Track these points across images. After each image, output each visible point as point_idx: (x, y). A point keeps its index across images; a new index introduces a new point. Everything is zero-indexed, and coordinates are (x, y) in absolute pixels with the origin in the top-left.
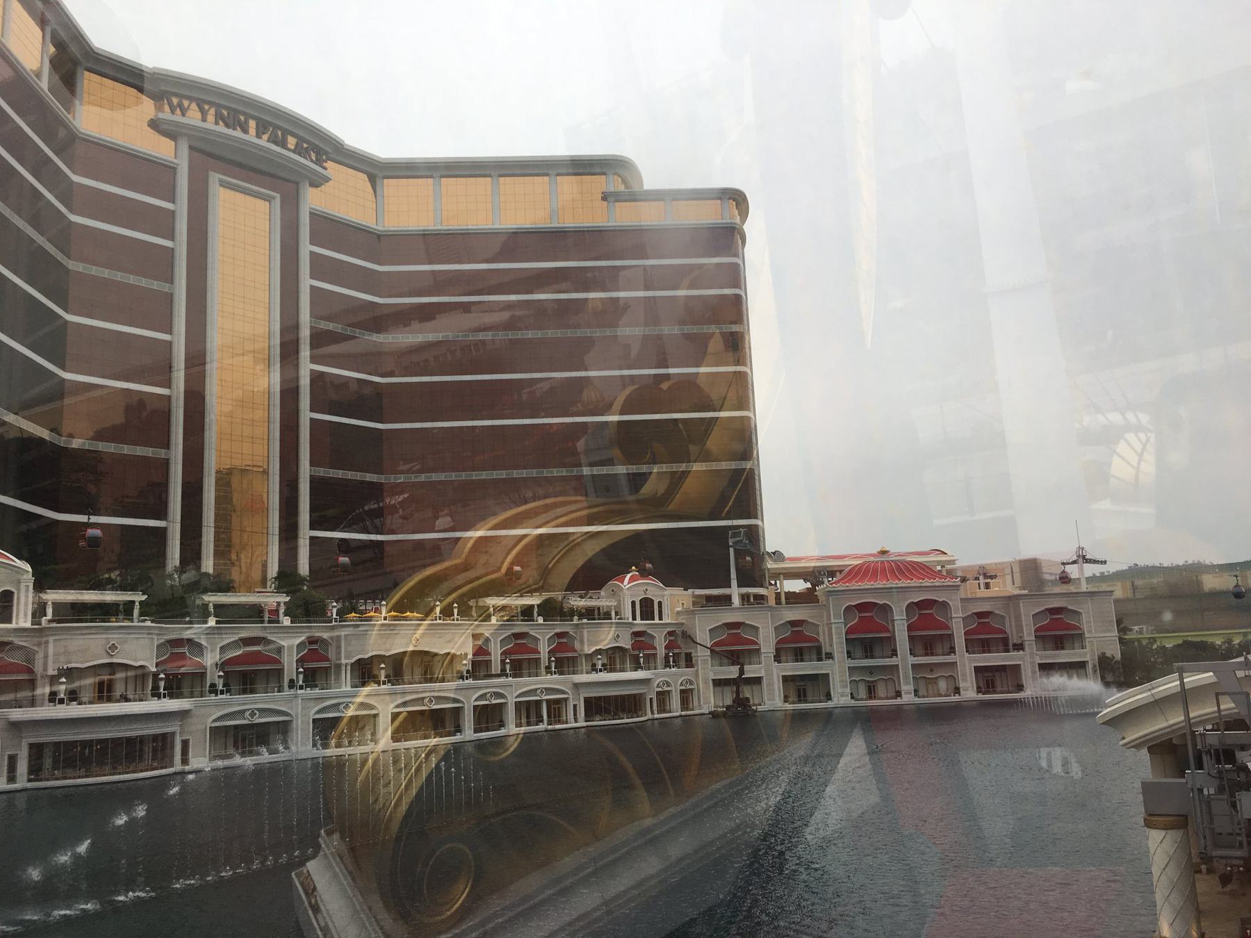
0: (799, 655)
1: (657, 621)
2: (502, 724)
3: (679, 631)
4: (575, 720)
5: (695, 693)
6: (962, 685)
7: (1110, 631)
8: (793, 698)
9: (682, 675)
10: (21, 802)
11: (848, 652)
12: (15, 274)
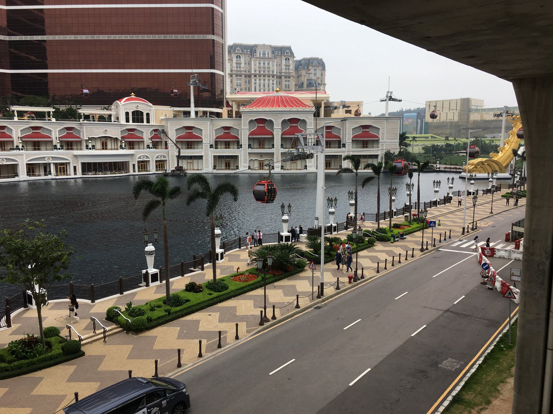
0: (36, 146)
1: (145, 123)
2: (16, 175)
3: (160, 129)
4: (75, 174)
5: (168, 162)
9: (158, 153)
10: (80, 181)
11: (282, 145)
12: (207, 8)
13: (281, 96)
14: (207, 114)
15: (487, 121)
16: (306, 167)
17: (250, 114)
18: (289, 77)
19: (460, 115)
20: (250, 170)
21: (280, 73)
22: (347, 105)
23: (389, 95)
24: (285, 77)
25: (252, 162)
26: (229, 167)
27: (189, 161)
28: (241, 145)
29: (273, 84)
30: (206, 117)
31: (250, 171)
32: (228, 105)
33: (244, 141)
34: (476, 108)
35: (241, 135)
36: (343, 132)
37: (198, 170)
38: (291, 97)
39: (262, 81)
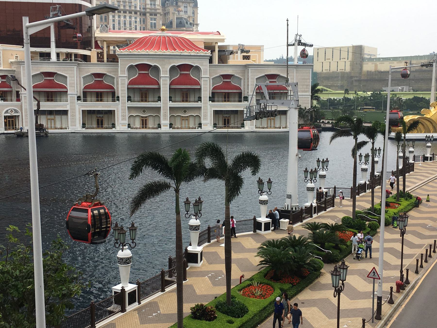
0: (227, 97)
3: (9, 75)
5: (20, 118)
6: (203, 122)
7: (306, 92)
8: (221, 124)
9: (8, 106)
11: (170, 97)
13: (167, 36)
14: (71, 57)
15: (382, 72)
16: (200, 125)
17: (128, 58)
18: (156, 15)
19: (352, 64)
20: (129, 129)
21: (144, 9)
22: (246, 49)
23: (298, 38)
24: (151, 15)
25: (132, 119)
26: (102, 124)
27: (49, 117)
28: (118, 97)
29: (136, 22)
30: (71, 60)
31: (130, 130)
32: (97, 47)
33: (122, 90)
34: (369, 57)
35: (118, 84)
36: (244, 82)
37: (61, 129)
38: (181, 38)
39: (122, 18)
